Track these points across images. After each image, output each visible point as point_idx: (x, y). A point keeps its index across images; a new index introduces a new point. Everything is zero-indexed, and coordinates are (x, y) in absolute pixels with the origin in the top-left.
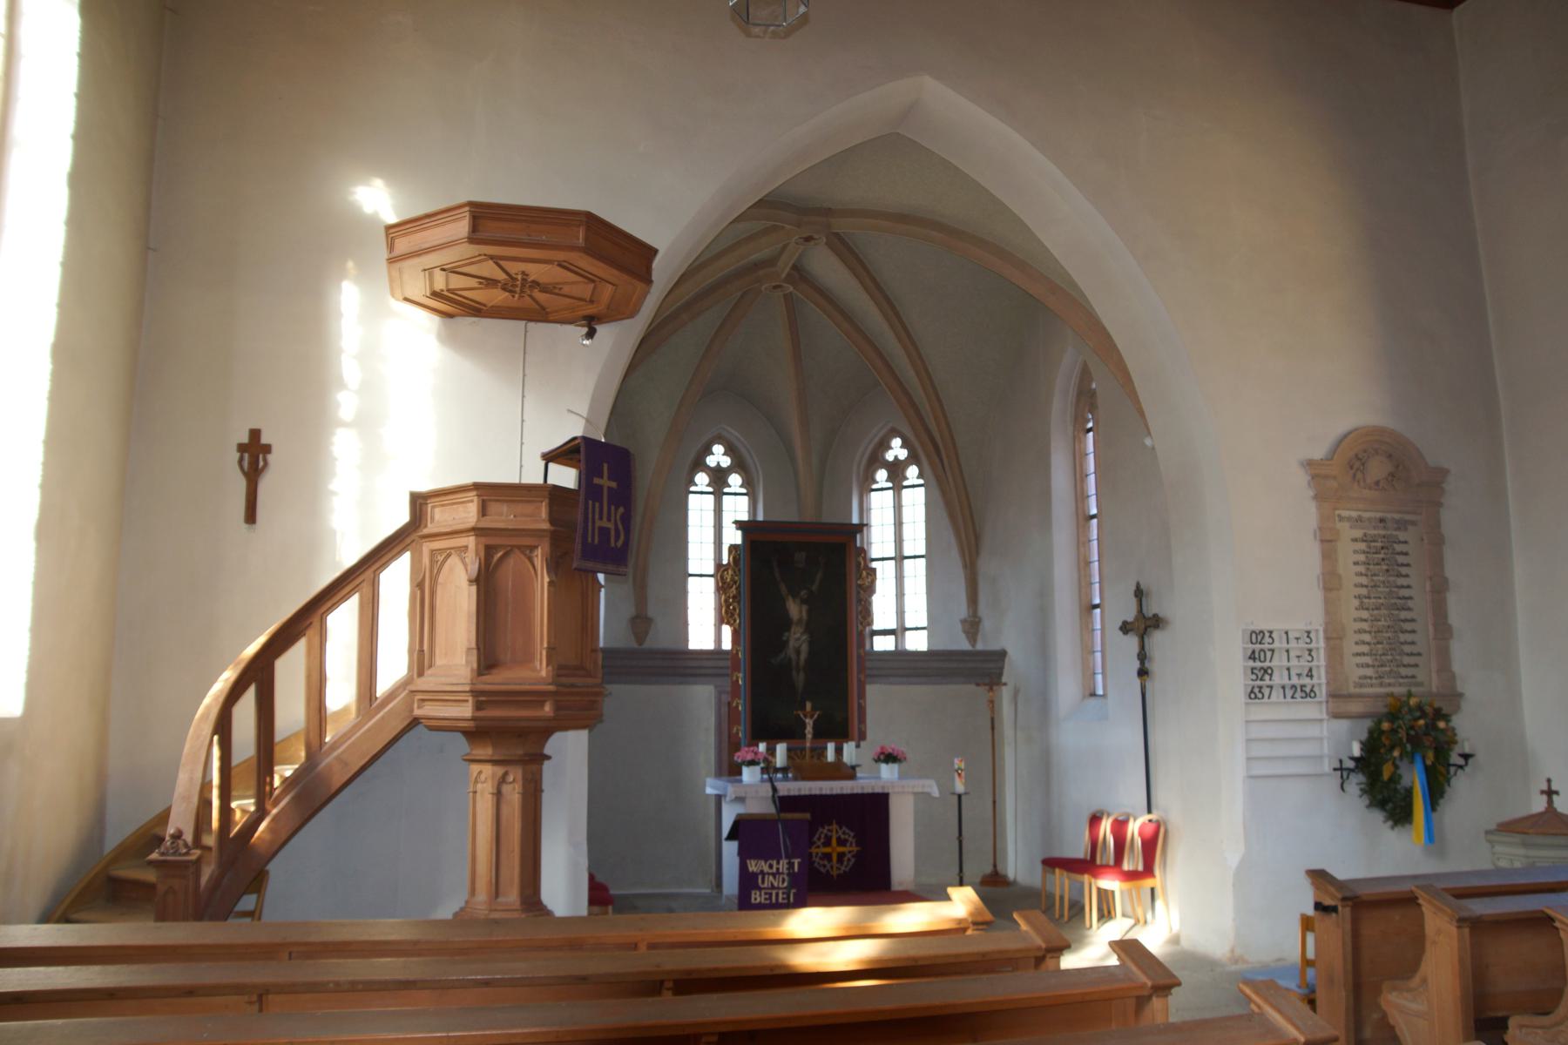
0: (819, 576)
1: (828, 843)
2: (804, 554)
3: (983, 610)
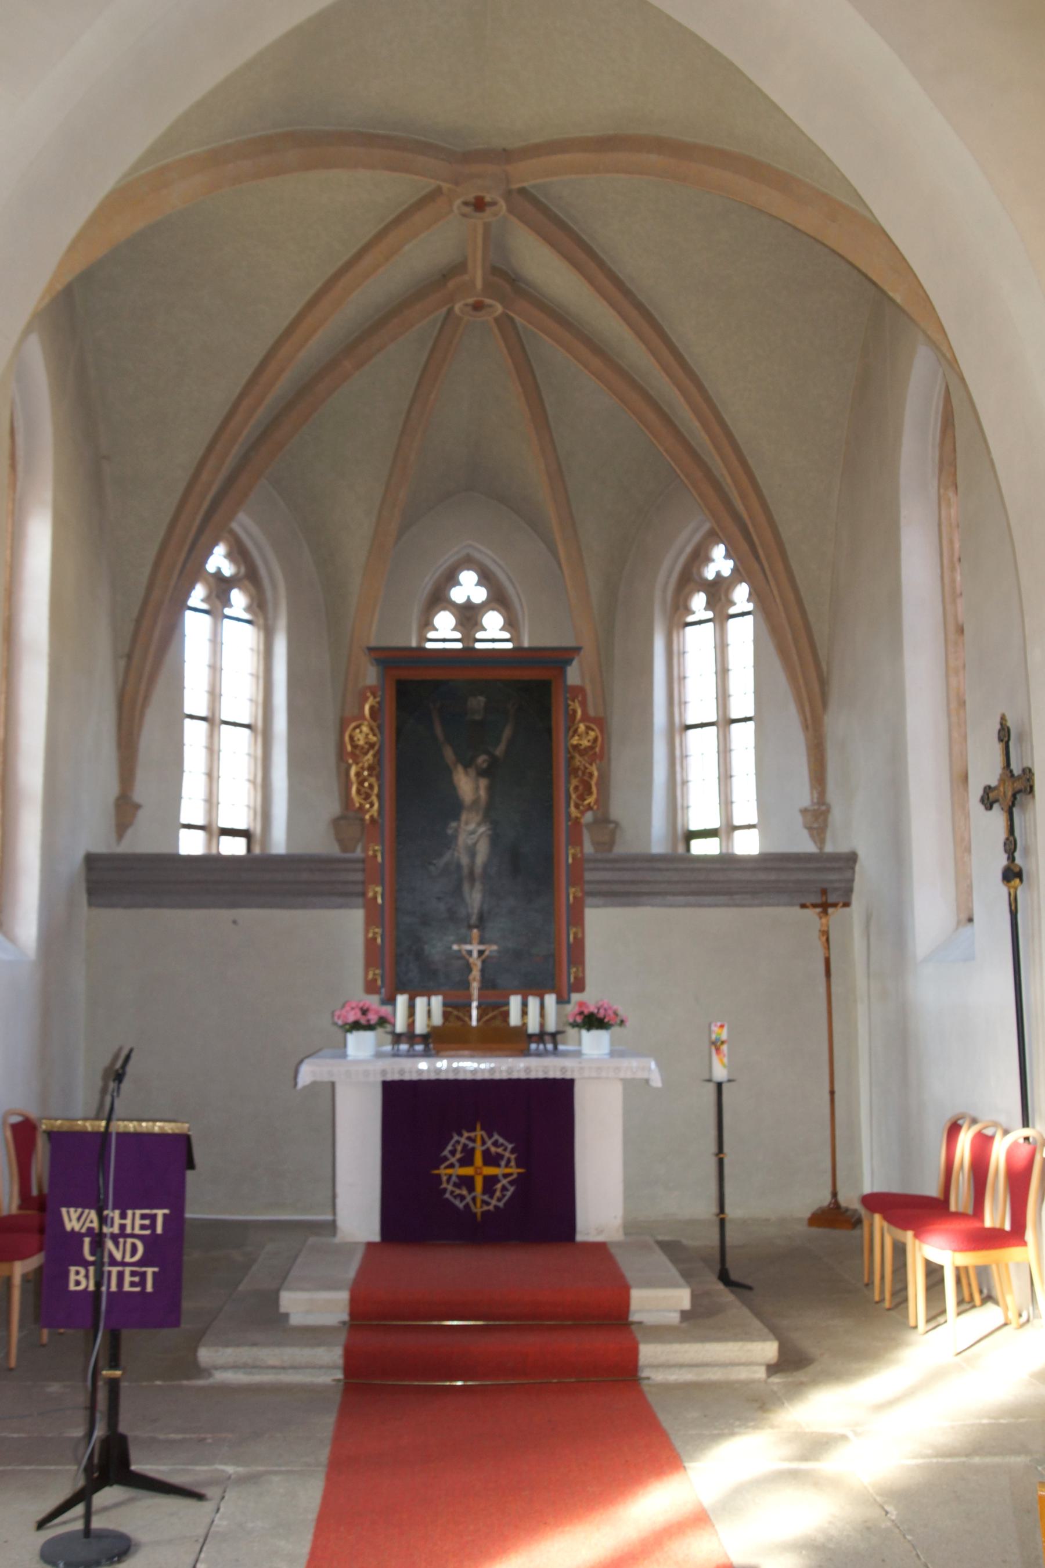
0: (507, 733)
1: (467, 1159)
2: (482, 699)
3: (833, 795)
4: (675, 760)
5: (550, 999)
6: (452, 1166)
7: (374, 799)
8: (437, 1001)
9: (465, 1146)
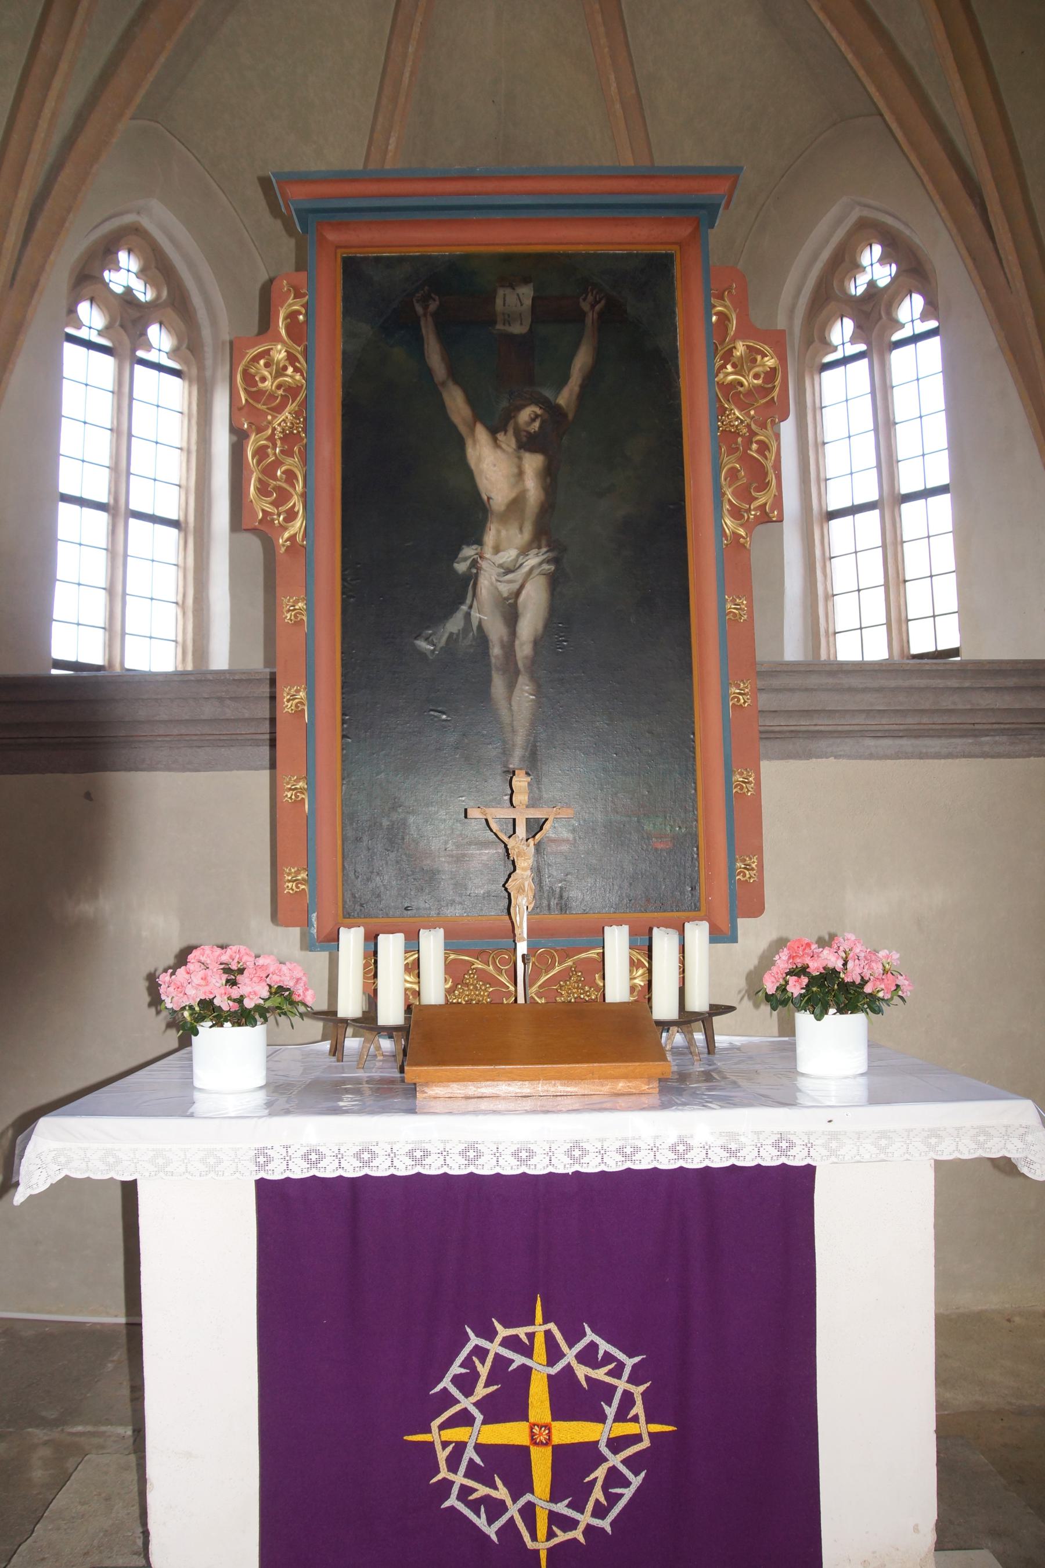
0: (581, 361)
2: (527, 292)
4: (815, 563)
5: (697, 933)
6: (464, 1419)
7: (296, 502)
8: (432, 945)
9: (501, 1362)
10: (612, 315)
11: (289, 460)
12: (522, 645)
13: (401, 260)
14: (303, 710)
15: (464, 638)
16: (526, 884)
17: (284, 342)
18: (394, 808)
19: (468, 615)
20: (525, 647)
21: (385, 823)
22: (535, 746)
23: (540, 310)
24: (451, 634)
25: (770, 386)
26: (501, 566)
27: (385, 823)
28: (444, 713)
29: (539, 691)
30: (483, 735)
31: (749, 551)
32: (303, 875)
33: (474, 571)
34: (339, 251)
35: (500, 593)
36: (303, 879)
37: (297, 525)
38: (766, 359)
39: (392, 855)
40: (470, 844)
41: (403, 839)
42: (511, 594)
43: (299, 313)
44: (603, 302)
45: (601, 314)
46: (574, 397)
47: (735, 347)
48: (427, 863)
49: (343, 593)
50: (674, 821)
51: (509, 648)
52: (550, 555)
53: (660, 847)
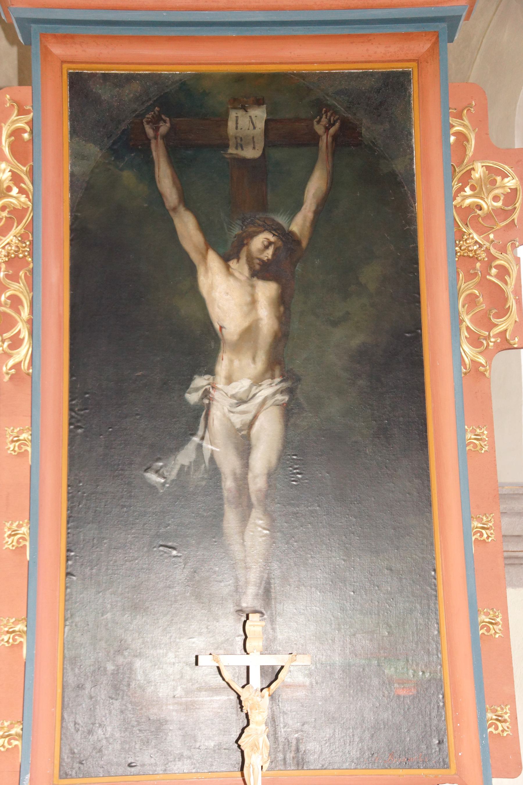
0: (316, 186)
2: (259, 115)
7: (22, 328)
10: (347, 137)
11: (15, 285)
12: (255, 477)
13: (130, 78)
14: (25, 546)
15: (195, 471)
16: (261, 740)
17: (7, 161)
18: (119, 652)
19: (200, 447)
20: (258, 480)
21: (110, 667)
22: (268, 583)
23: (276, 133)
24: (183, 466)
25: (510, 208)
26: (233, 396)
27: (110, 667)
28: (174, 548)
29: (272, 527)
30: (215, 572)
31: (489, 379)
32: (17, 730)
33: (206, 401)
34: (65, 66)
35: (232, 425)
36: (17, 734)
37: (22, 354)
38: (506, 180)
39: (117, 704)
40: (200, 690)
41: (129, 685)
42: (244, 425)
43: (24, 131)
44: (337, 125)
45: (335, 137)
46: (308, 224)
47: (473, 169)
48: (154, 712)
49: (70, 424)
50: (417, 665)
51: (242, 481)
52: (284, 385)
53: (402, 693)
